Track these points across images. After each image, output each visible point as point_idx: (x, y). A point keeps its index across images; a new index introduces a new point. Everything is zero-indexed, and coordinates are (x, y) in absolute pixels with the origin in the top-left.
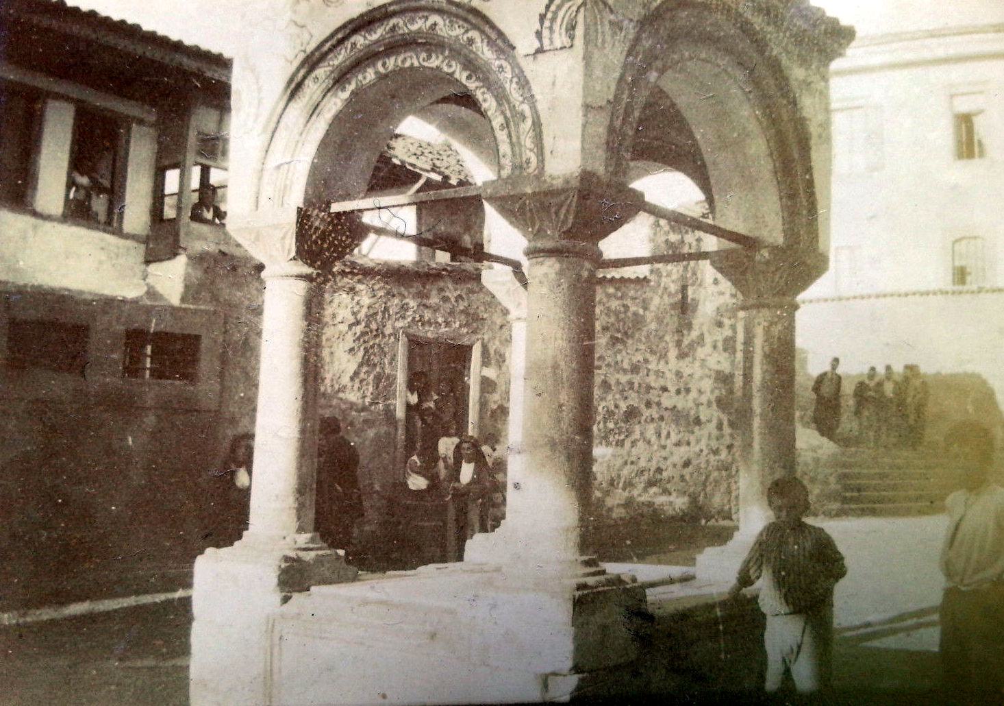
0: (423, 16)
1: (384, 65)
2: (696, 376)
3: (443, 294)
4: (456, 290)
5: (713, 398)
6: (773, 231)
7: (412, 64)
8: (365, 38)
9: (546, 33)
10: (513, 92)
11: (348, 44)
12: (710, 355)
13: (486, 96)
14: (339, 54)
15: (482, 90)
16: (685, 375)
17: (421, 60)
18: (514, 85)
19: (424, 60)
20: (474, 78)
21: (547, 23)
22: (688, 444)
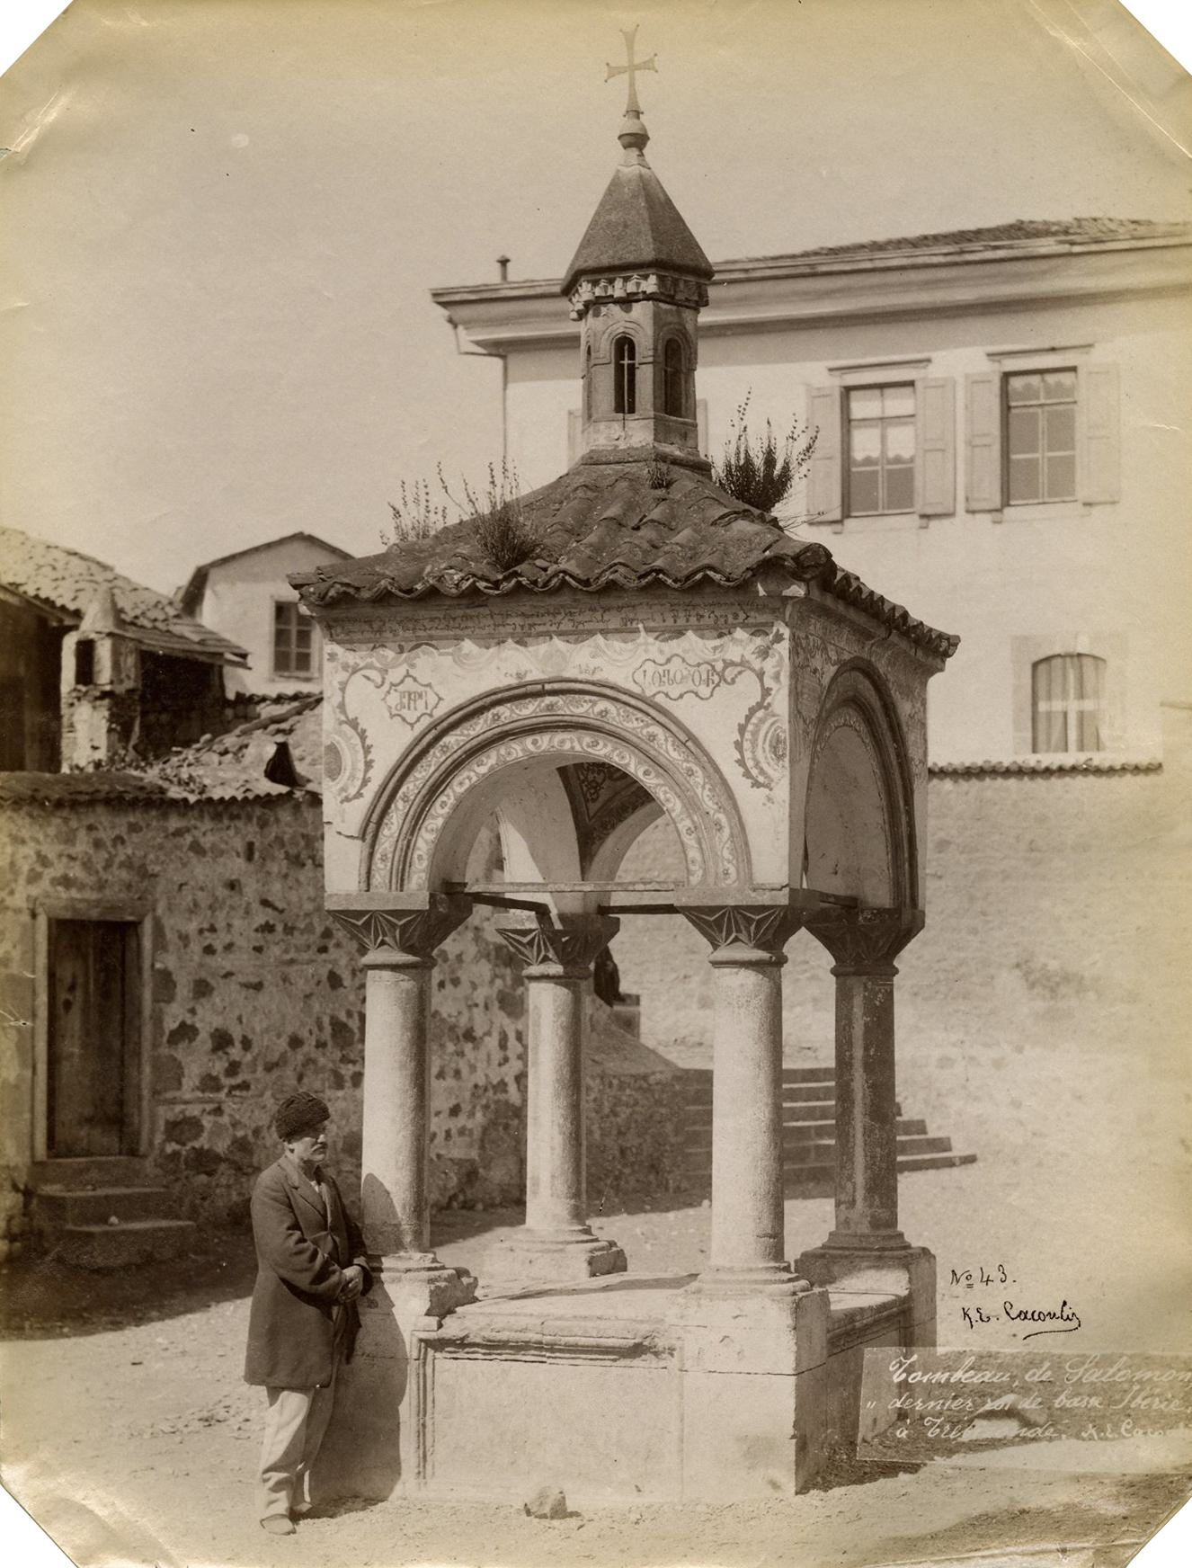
0: (590, 701)
1: (535, 743)
2: (467, 958)
3: (94, 834)
4: (113, 828)
5: (494, 992)
6: (878, 894)
7: (573, 748)
8: (512, 711)
9: (747, 745)
10: (706, 799)
11: (489, 715)
12: (488, 919)
13: (668, 795)
14: (476, 724)
15: (663, 789)
16: (451, 957)
17: (584, 745)
18: (707, 792)
19: (588, 746)
20: (653, 774)
21: (748, 735)
22: (457, 1073)
